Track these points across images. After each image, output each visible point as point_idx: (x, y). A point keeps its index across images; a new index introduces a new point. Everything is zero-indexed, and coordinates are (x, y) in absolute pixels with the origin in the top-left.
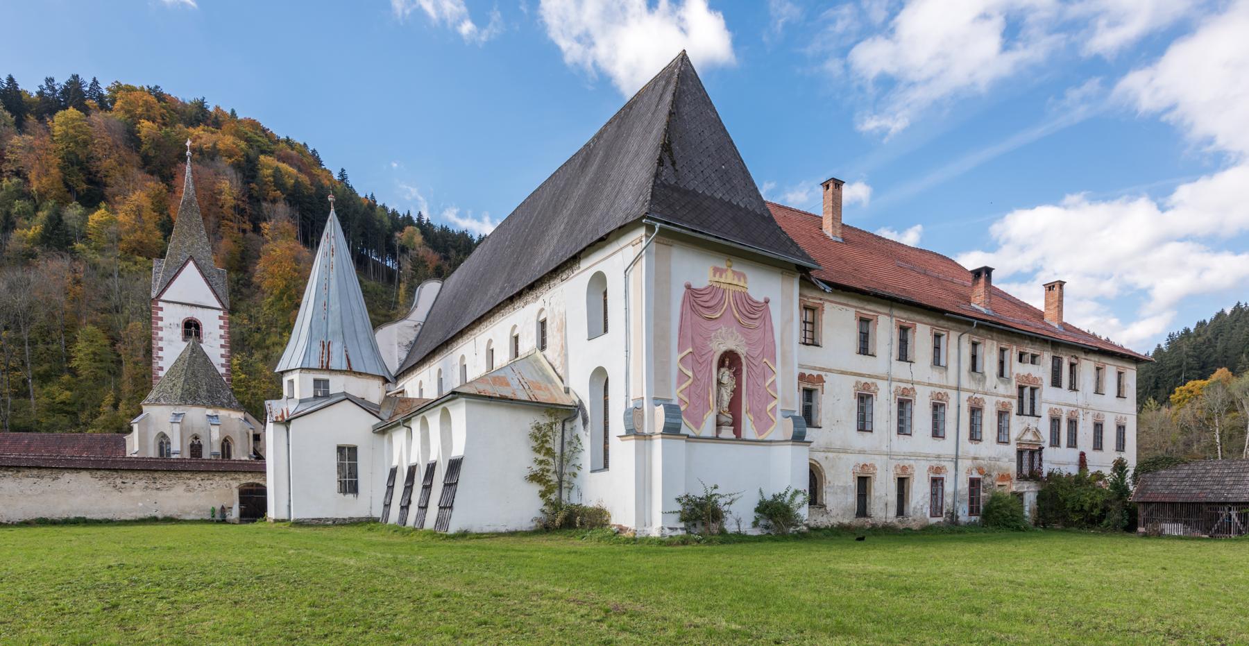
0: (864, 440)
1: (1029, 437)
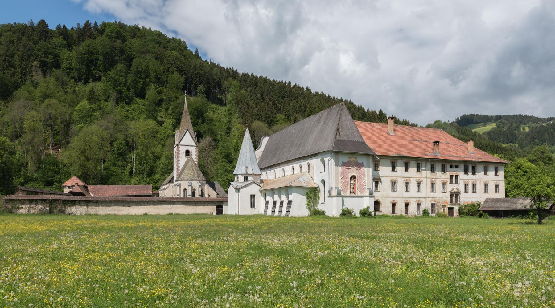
0: (394, 194)
1: (455, 190)
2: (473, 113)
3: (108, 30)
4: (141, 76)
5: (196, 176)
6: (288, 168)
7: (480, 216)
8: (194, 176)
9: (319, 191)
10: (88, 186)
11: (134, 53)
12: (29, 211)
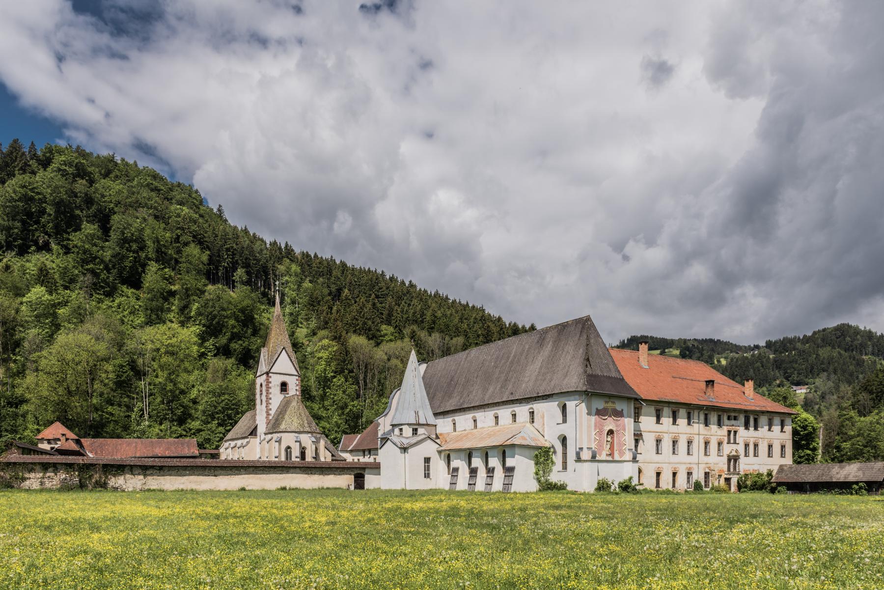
0: (658, 458)
1: (734, 453)
2: (646, 334)
3: (58, 160)
4: (131, 247)
5: (306, 425)
6: (485, 418)
7: (773, 491)
8: (302, 426)
9: (555, 452)
10: (82, 440)
11: (112, 205)
12: (42, 483)
